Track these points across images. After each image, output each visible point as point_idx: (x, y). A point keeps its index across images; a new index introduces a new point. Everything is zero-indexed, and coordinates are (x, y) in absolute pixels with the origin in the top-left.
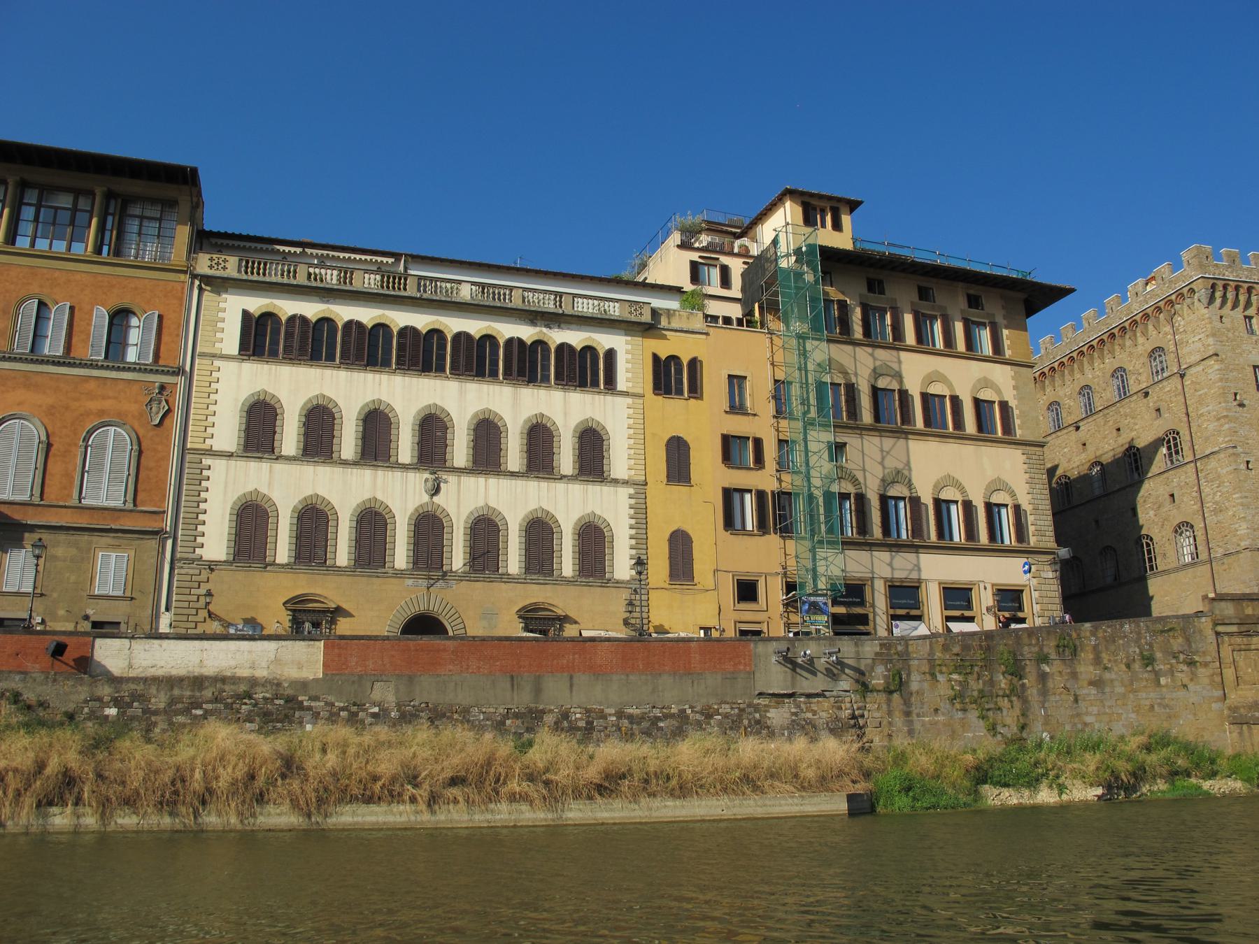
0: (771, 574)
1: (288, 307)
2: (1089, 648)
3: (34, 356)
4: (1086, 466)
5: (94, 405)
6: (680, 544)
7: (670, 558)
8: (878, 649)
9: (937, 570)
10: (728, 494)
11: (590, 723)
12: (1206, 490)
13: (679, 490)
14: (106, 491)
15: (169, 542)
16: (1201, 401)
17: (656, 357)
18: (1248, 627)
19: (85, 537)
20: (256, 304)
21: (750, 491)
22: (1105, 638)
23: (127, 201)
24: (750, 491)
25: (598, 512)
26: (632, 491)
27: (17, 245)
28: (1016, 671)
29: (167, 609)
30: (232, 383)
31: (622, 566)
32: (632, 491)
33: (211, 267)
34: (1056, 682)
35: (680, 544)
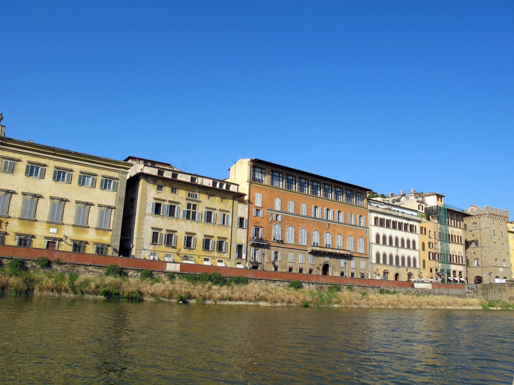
3: (360, 226)
5: (359, 234)
9: (453, 267)
10: (429, 253)
12: (483, 253)
13: (423, 252)
14: (361, 250)
16: (484, 236)
18: (511, 285)
19: (359, 258)
28: (487, 290)
29: (240, 247)
30: (375, 230)
34: (490, 292)
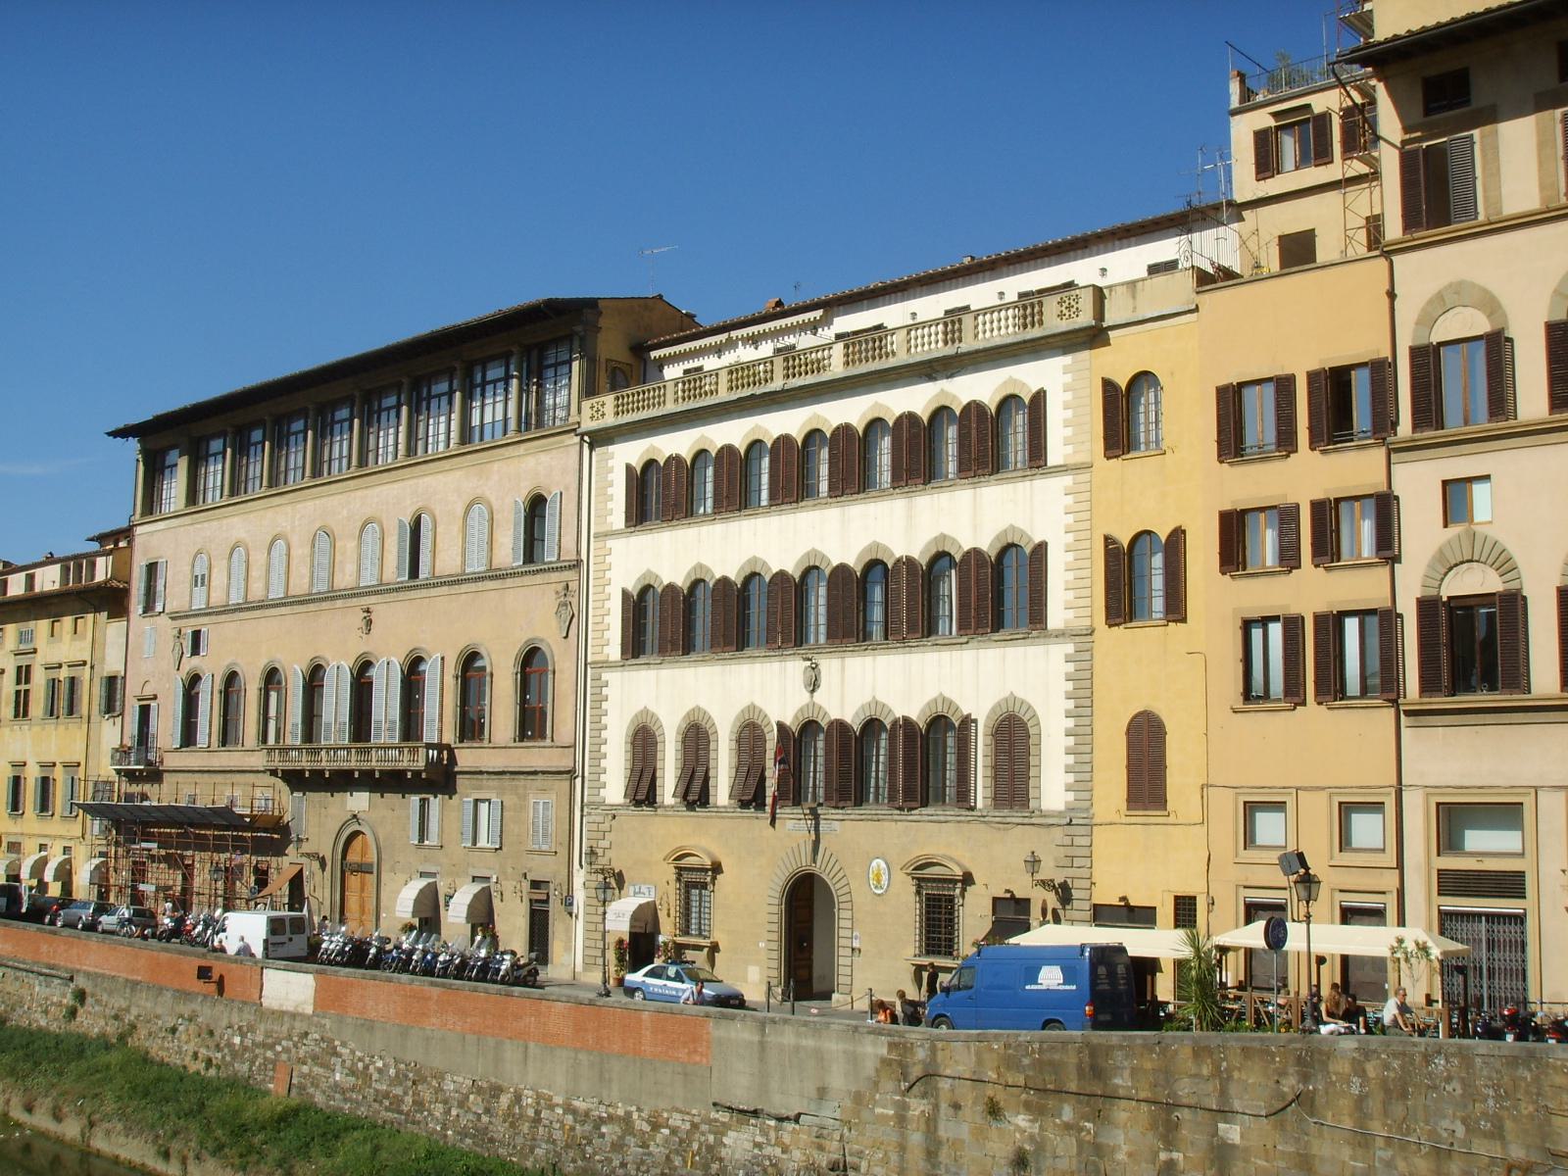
0: (1305, 789)
1: (679, 444)
2: (1345, 1103)
4: (970, 645)
6: (1146, 740)
8: (884, 1051)
11: (538, 1113)
15: (579, 781)
17: (1108, 385)
20: (631, 453)
21: (1276, 619)
22: (1384, 1081)
23: (542, 348)
25: (1020, 695)
26: (1070, 648)
31: (1053, 788)
32: (1070, 648)
33: (1061, 315)
35: (1146, 740)
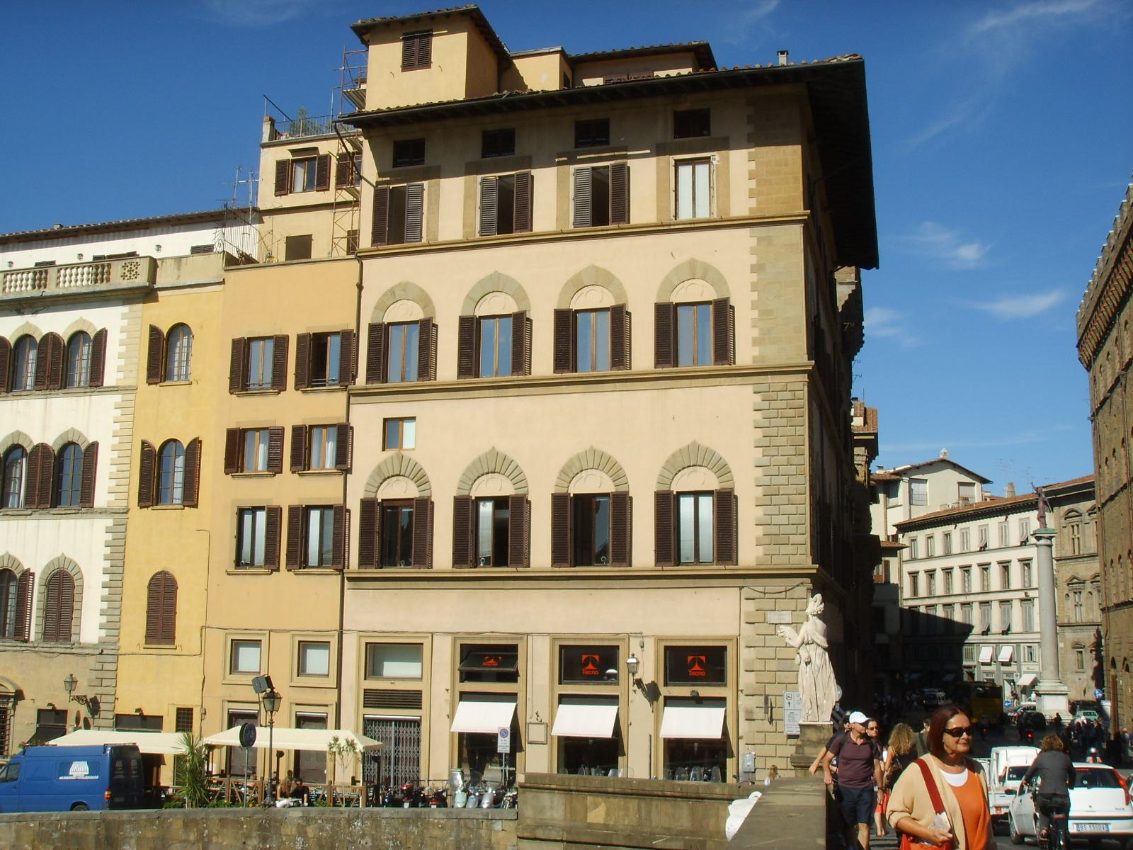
0: (276, 631)
6: (163, 592)
7: (148, 612)
17: (154, 331)
21: (262, 508)
24: (262, 508)
26: (110, 522)
27: (631, 223)
31: (90, 625)
32: (110, 522)
33: (124, 276)
35: (163, 592)
